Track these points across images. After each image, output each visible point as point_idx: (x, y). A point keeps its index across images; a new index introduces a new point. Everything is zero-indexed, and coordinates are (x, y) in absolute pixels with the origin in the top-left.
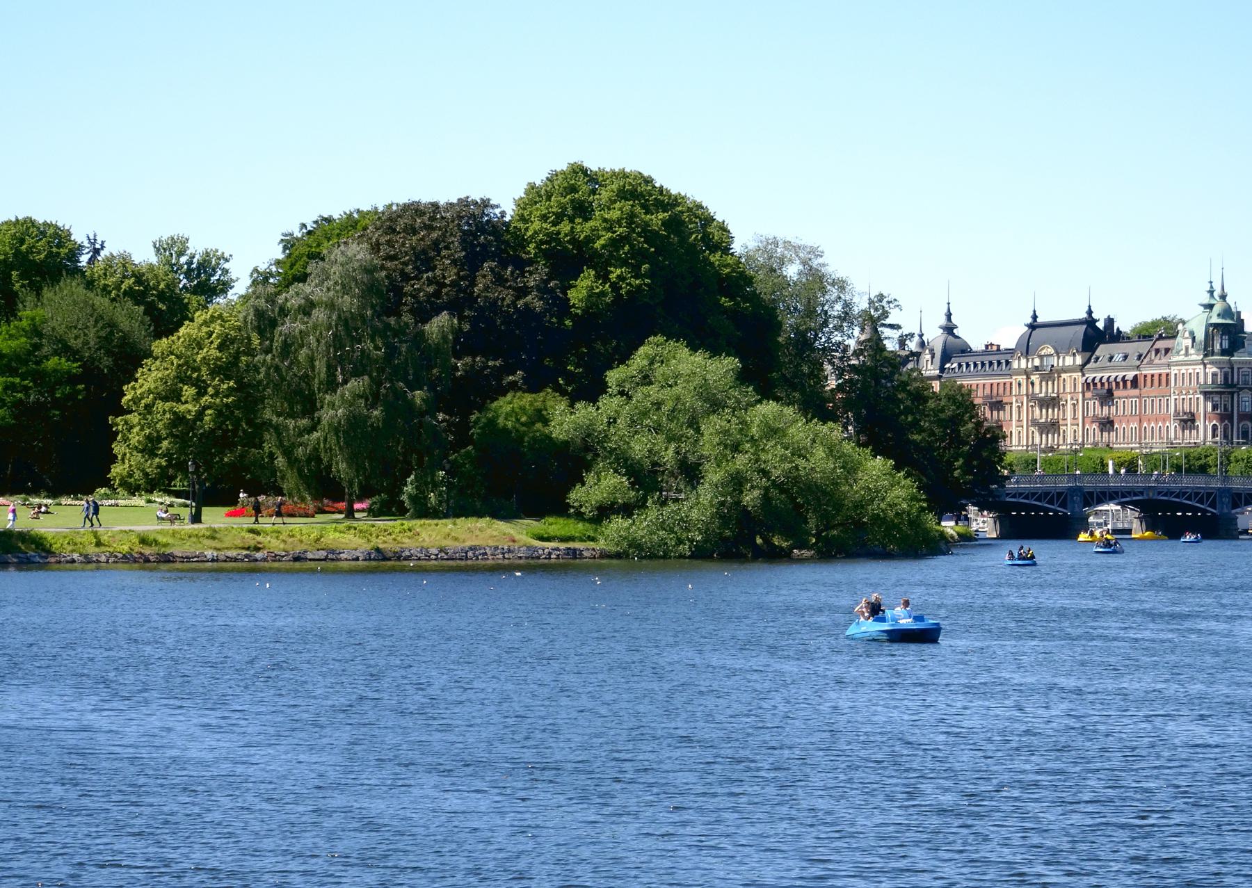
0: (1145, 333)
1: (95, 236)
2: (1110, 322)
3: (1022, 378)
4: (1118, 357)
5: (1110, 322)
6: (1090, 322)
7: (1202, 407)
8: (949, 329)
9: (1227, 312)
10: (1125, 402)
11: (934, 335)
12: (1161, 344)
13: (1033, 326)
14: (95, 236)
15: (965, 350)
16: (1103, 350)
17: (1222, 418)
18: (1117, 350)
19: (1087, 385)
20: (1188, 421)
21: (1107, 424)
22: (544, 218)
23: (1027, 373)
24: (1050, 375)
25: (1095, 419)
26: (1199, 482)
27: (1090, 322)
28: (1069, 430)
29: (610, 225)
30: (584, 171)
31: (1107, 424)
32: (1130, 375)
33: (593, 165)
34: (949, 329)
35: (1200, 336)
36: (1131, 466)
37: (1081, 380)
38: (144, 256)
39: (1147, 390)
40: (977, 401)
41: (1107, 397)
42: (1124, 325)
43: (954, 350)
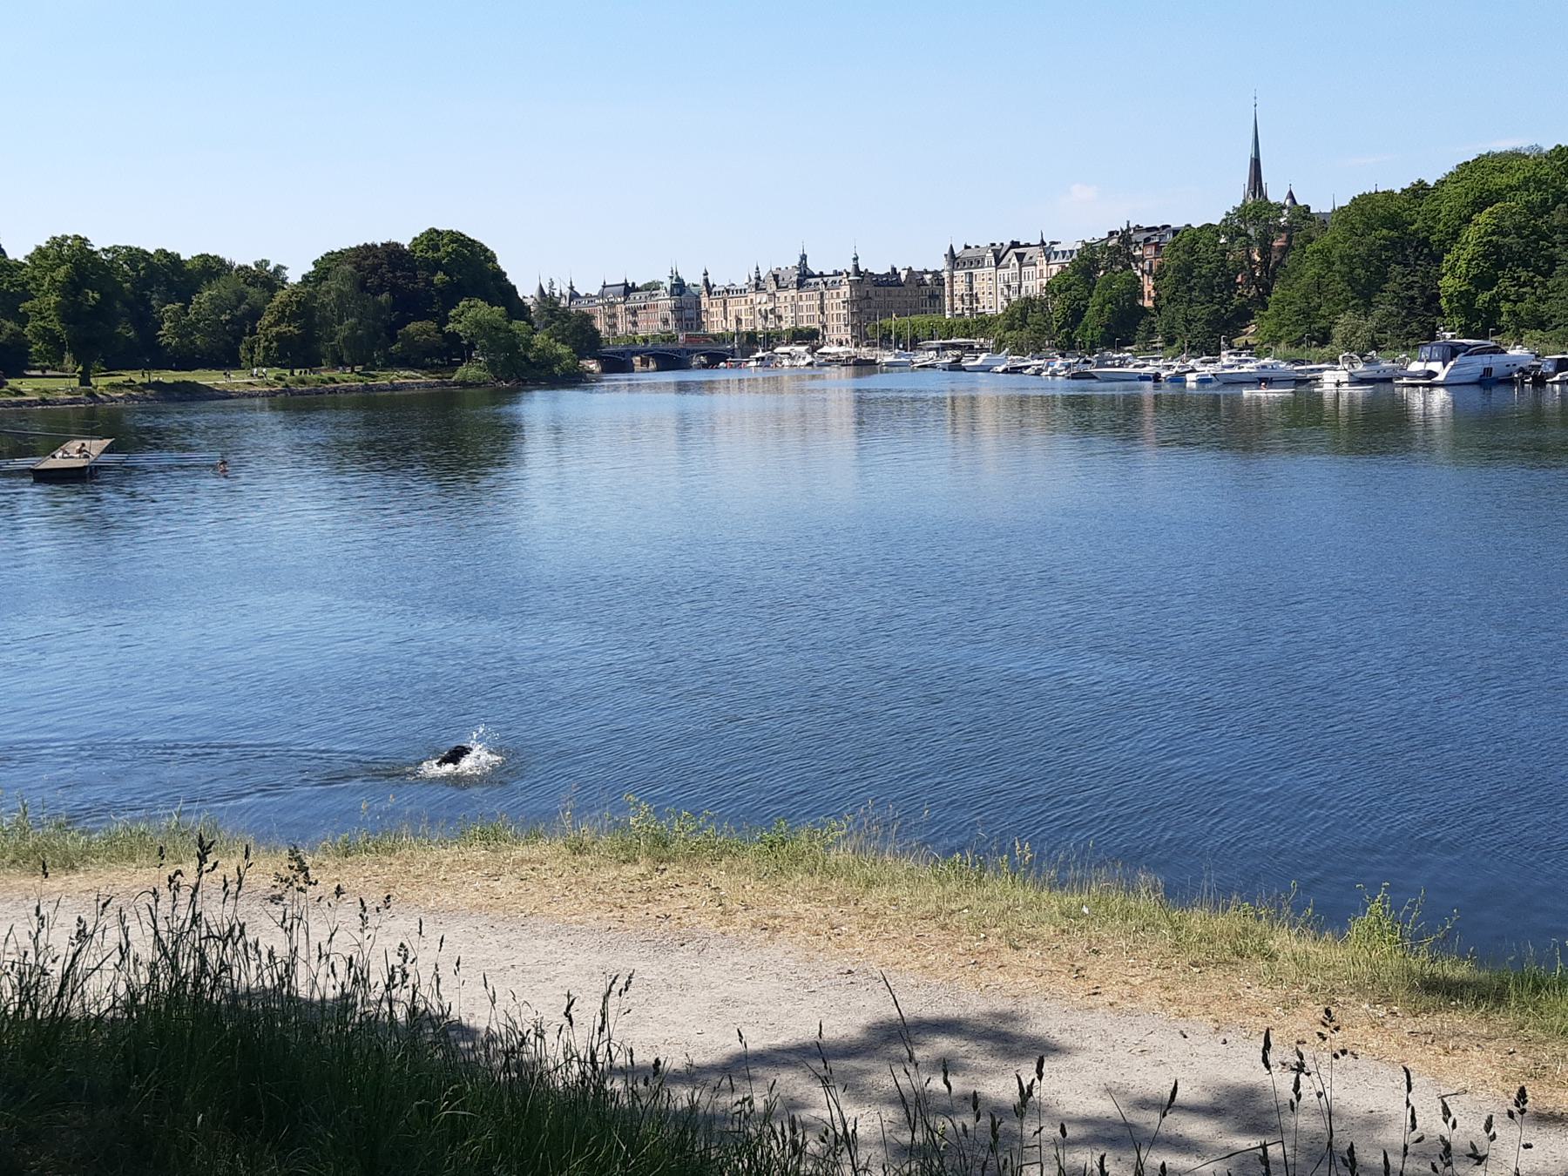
0: (647, 287)
1: (552, 283)
2: (633, 284)
3: (601, 307)
4: (643, 297)
5: (633, 284)
6: (626, 284)
7: (670, 317)
8: (572, 288)
9: (678, 279)
10: (641, 316)
11: (566, 291)
12: (654, 292)
13: (604, 287)
14: (552, 283)
15: (578, 296)
16: (632, 296)
17: (678, 320)
18: (637, 295)
19: (626, 309)
20: (666, 322)
21: (635, 324)
22: (421, 251)
23: (602, 305)
24: (612, 305)
25: (630, 322)
26: (670, 346)
27: (626, 284)
28: (620, 326)
29: (448, 254)
30: (436, 231)
31: (635, 324)
32: (643, 305)
33: (440, 228)
34: (572, 288)
35: (669, 289)
36: (645, 340)
37: (624, 307)
38: (312, 268)
39: (649, 311)
40: (990, 1024)
41: (634, 313)
42: (638, 285)
43: (574, 296)
